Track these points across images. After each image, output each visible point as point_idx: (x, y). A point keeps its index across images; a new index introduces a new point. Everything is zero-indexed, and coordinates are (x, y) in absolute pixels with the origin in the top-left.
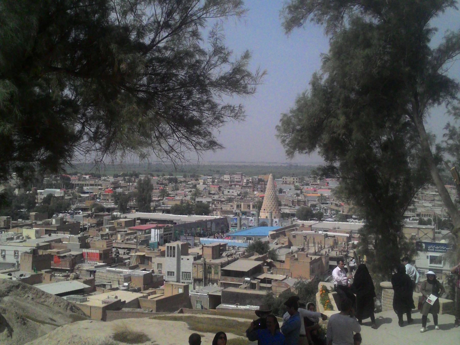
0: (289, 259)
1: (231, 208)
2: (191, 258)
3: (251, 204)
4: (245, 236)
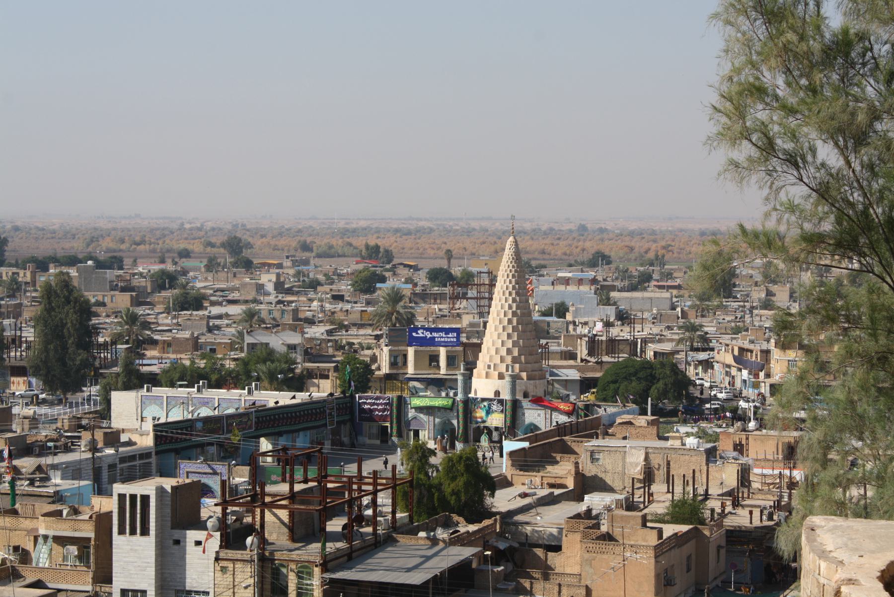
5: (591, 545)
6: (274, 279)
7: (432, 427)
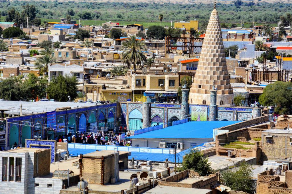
0: (267, 185)
1: (124, 86)
2: (57, 182)
3: (167, 78)
4: (161, 140)
5: (277, 190)
6: (59, 33)
7: (166, 121)
